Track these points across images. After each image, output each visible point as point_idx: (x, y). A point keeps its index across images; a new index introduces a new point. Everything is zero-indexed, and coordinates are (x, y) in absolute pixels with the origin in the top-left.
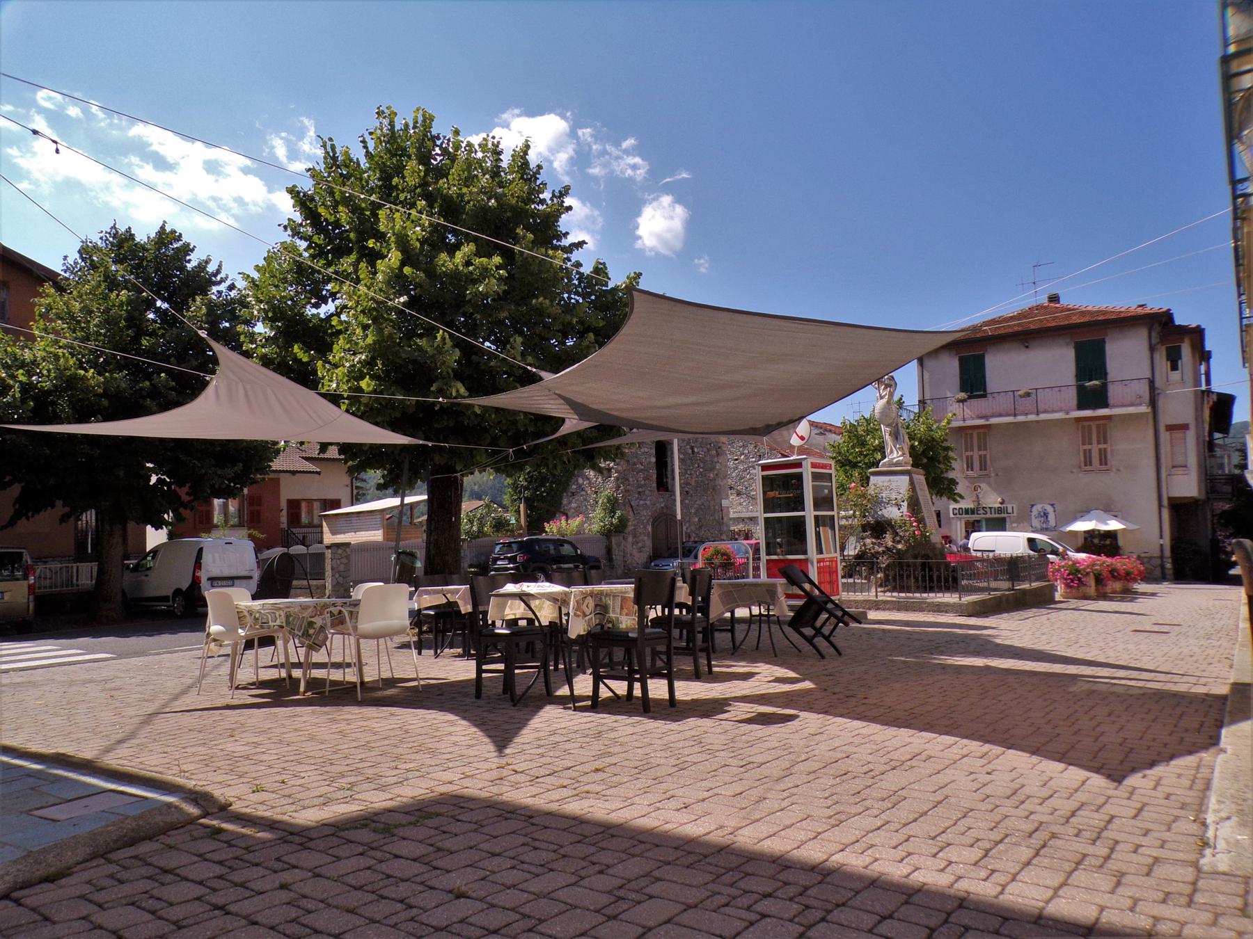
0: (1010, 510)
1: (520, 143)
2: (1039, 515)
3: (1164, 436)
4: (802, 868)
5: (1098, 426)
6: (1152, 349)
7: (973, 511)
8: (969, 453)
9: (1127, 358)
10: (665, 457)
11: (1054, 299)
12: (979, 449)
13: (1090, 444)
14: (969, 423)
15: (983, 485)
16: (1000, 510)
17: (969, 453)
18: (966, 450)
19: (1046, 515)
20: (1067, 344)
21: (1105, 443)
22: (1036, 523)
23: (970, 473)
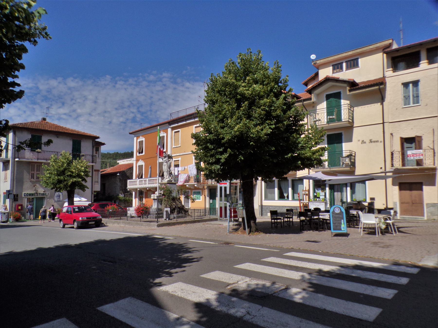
0: (47, 194)
1: (193, 146)
2: (57, 196)
3: (94, 172)
4: (393, 52)
5: (37, 165)
6: (93, 147)
7: (32, 195)
8: (33, 172)
9: (86, 148)
10: (347, 174)
11: (44, 119)
12: (37, 171)
13: (34, 171)
14: (34, 160)
15: (37, 185)
16: (43, 194)
17: (33, 172)
18: (32, 171)
19: (59, 196)
20: (70, 140)
21: (39, 171)
22: (56, 199)
23: (32, 180)
